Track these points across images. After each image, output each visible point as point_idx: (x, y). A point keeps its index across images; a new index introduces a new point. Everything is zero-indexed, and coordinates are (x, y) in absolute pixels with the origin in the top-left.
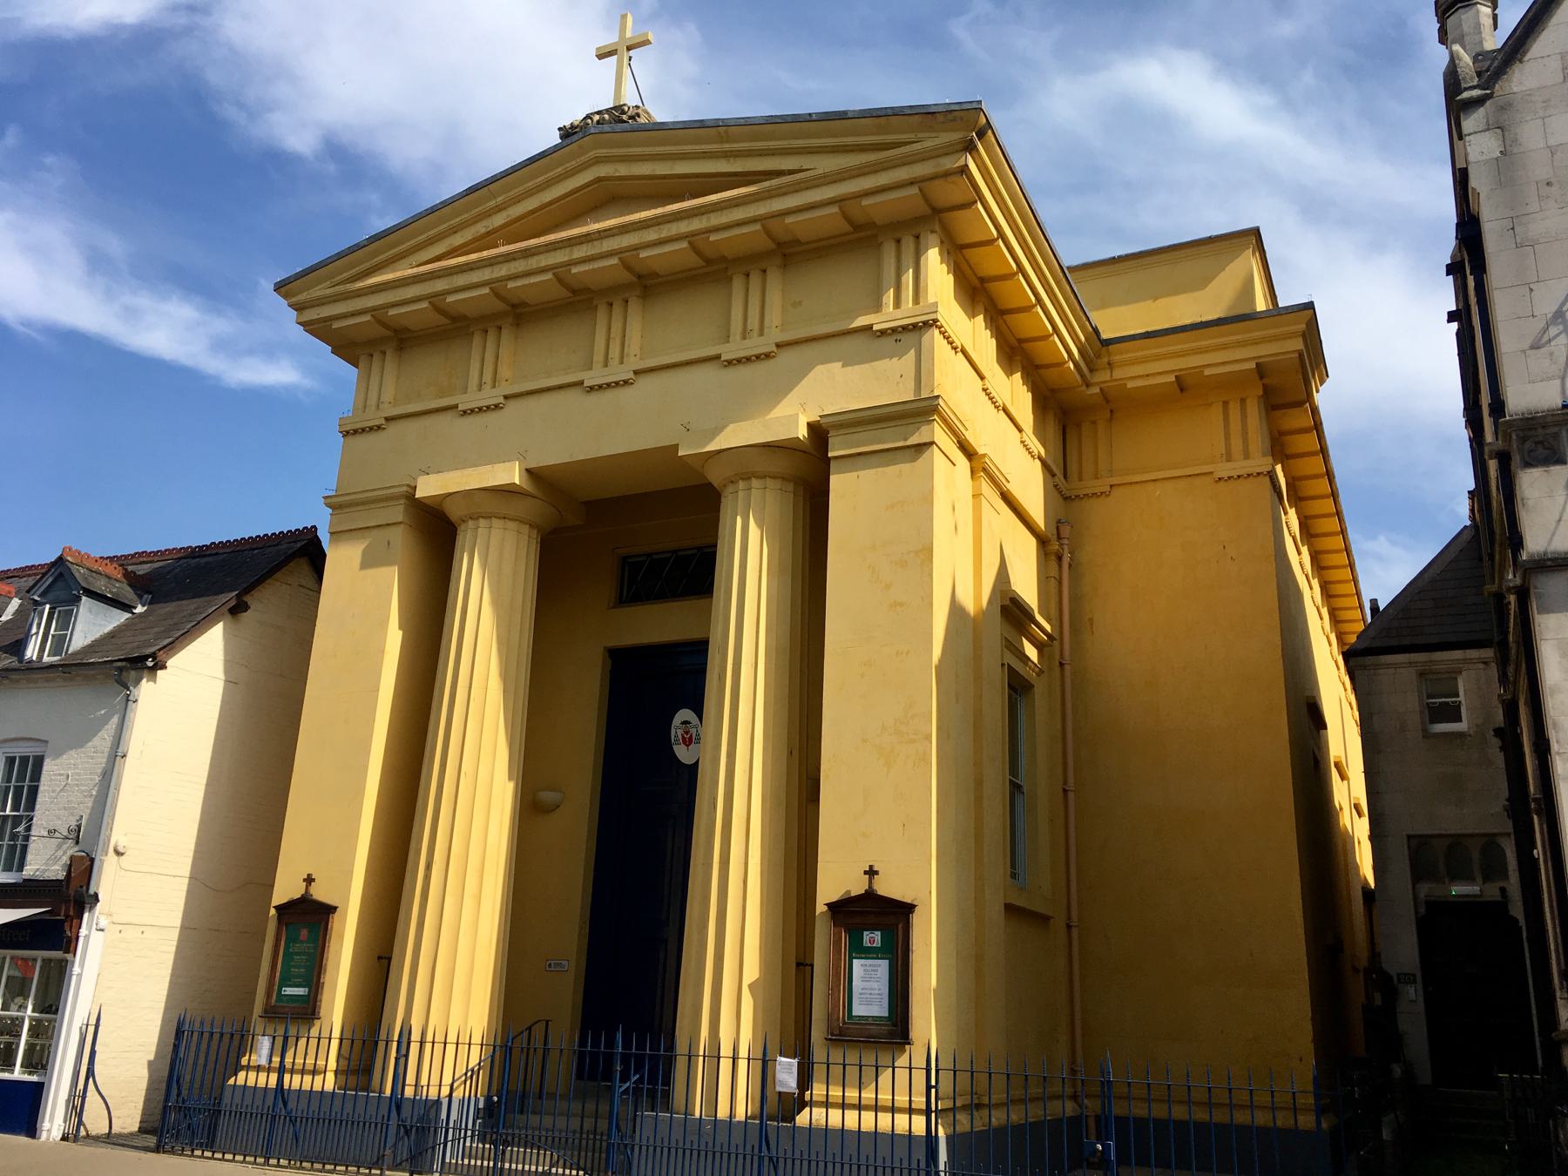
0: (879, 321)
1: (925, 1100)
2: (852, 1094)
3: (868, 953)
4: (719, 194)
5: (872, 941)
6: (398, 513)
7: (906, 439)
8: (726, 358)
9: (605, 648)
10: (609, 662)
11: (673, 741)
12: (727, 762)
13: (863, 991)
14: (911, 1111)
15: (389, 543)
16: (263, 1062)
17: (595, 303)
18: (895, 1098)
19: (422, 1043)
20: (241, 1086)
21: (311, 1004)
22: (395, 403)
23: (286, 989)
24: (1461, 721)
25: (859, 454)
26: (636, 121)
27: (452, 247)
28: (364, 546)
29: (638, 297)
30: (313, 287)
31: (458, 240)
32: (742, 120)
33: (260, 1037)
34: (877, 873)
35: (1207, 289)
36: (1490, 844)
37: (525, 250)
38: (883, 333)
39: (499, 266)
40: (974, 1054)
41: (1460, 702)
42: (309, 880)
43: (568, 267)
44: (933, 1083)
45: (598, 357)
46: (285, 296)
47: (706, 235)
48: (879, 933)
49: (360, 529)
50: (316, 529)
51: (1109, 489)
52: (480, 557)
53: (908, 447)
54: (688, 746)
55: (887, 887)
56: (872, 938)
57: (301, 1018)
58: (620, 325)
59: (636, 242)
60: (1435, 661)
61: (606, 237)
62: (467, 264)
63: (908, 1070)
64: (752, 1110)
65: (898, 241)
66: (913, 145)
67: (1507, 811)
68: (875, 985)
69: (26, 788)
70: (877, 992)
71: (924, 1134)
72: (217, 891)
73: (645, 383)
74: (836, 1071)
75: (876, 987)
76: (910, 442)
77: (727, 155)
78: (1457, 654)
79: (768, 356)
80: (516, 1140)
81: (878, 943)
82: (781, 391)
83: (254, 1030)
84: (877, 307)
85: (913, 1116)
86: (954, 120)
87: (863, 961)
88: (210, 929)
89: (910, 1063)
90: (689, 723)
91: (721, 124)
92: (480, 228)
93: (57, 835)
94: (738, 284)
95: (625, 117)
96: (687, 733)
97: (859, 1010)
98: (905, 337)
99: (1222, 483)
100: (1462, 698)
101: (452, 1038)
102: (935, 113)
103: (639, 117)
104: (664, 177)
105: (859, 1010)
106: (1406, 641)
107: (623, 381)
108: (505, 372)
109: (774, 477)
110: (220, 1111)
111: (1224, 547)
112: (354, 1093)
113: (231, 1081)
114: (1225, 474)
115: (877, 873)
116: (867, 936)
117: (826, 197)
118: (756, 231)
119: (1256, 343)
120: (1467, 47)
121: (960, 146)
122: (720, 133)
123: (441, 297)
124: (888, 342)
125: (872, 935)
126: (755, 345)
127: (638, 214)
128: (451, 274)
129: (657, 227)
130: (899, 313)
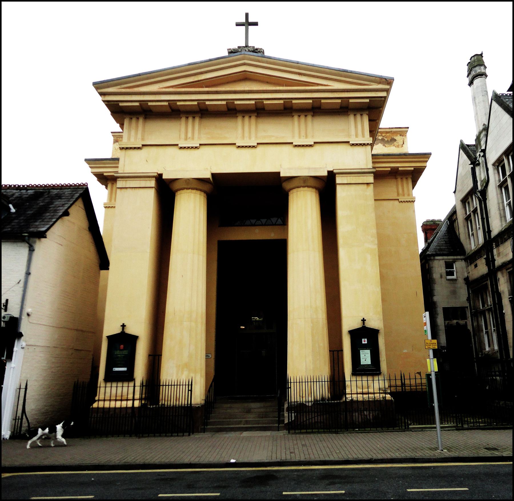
1: (346, 391)
6: (152, 183)
24: (454, 276)
29: (367, 114)
41: (454, 270)
46: (97, 89)
56: (365, 341)
66: (369, 86)
79: (311, 146)
88: (55, 347)
120: (244, 48)
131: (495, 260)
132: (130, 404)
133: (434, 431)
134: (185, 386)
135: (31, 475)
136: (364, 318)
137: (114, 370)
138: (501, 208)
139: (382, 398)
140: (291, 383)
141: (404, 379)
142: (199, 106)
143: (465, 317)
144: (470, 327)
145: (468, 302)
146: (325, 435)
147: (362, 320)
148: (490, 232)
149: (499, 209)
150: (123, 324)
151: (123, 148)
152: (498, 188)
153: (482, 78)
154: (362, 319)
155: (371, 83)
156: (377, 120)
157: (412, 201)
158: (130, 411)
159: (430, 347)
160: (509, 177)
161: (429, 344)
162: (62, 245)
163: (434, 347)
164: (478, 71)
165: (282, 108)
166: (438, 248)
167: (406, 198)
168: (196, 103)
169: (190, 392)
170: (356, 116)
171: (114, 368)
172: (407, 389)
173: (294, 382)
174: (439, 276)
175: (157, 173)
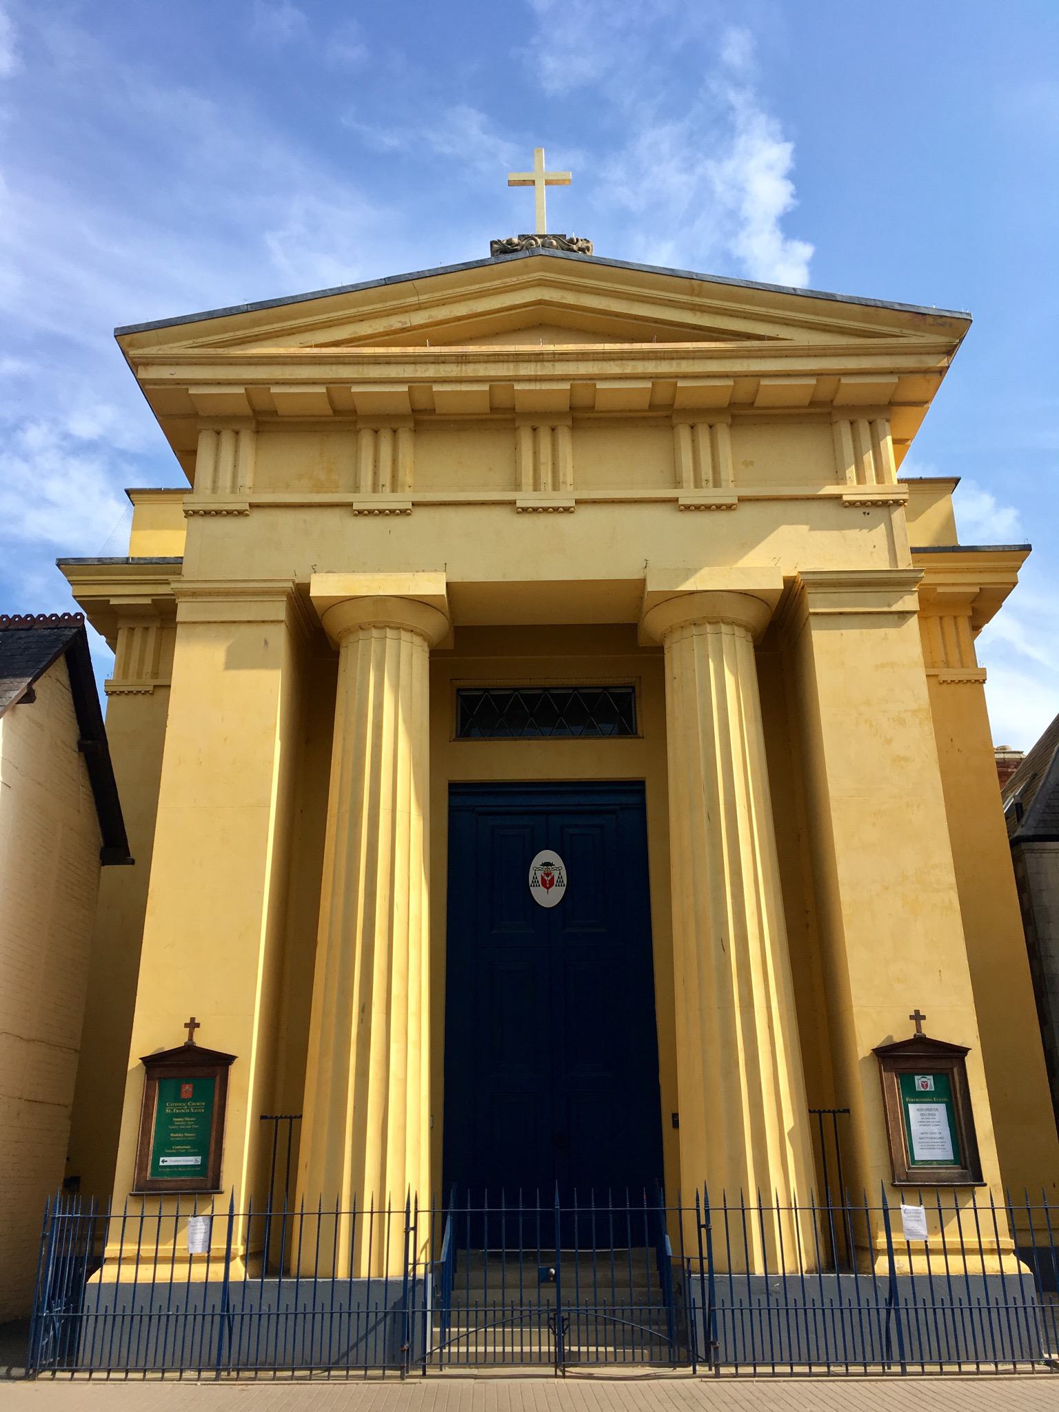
0: (850, 490)
2: (148, 1249)
3: (922, 1097)
4: (694, 343)
5: (925, 1085)
6: (279, 610)
7: (890, 606)
8: (683, 503)
11: (530, 883)
12: (732, 903)
13: (924, 1136)
14: (999, 1251)
15: (266, 643)
16: (198, 1249)
17: (675, 421)
18: (964, 1240)
19: (356, 1214)
20: (109, 1284)
21: (210, 1174)
22: (254, 489)
23: (166, 1159)
25: (841, 613)
26: (585, 253)
27: (357, 335)
28: (229, 644)
30: (165, 343)
31: (365, 329)
32: (718, 278)
33: (190, 1219)
34: (198, 1025)
35: (917, 521)
37: (462, 356)
38: (852, 504)
39: (424, 366)
40: (305, 1198)
42: (193, 1025)
43: (268, 386)
44: (703, 1230)
45: (527, 477)
47: (675, 380)
48: (931, 1077)
49: (222, 622)
51: (152, 689)
52: (731, 671)
53: (891, 613)
54: (548, 888)
55: (206, 1040)
56: (925, 1082)
57: (199, 1194)
58: (549, 451)
59: (597, 372)
61: (559, 361)
62: (631, 352)
63: (973, 1210)
64: (807, 1263)
65: (237, 433)
68: (935, 1129)
70: (938, 1136)
71: (222, 1280)
72: (29, 1041)
73: (585, 513)
74: (133, 1224)
75: (936, 1131)
76: (895, 608)
77: (694, 308)
80: (582, 1316)
81: (931, 1087)
82: (748, 543)
83: (390, 1207)
84: (840, 479)
85: (930, 1257)
86: (943, 325)
87: (918, 1106)
89: (992, 1203)
91: (695, 277)
92: (395, 322)
94: (366, 440)
95: (575, 247)
96: (548, 875)
97: (920, 1154)
98: (874, 511)
99: (945, 685)
101: (716, 1202)
102: (925, 314)
103: (588, 250)
104: (617, 315)
105: (920, 1154)
107: (389, 510)
108: (406, 477)
109: (739, 625)
110: (82, 1317)
111: (952, 740)
112: (296, 1280)
113: (94, 1278)
114: (949, 679)
115: (198, 1025)
116: (918, 1080)
117: (734, 370)
118: (727, 386)
119: (980, 572)
121: (944, 349)
122: (692, 285)
123: (346, 385)
124: (857, 514)
125: (923, 1080)
126: (387, 500)
127: (602, 345)
128: (363, 364)
129: (619, 362)
130: (862, 488)
132: (217, 1272)
134: (778, 1206)
137: (161, 1164)
139: (806, 1272)
141: (707, 1211)
142: (331, 402)
151: (195, 513)
154: (196, 1022)
156: (908, 440)
157: (944, 681)
158: (161, 1300)
162: (10, 787)
165: (485, 407)
167: (963, 674)
168: (240, 390)
170: (713, 428)
171: (161, 1159)
172: (952, 1243)
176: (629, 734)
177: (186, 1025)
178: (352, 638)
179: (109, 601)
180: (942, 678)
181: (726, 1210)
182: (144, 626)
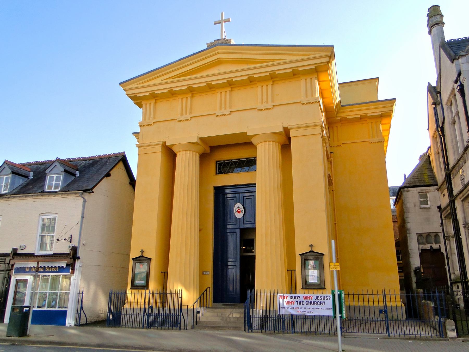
6: (160, 148)
9: (214, 187)
10: (214, 190)
36: (436, 235)
50: (125, 152)
60: (410, 190)
67: (441, 227)
69: (46, 227)
78: (428, 188)
89: (395, 296)
90: (240, 207)
93: (66, 240)
96: (239, 210)
97: (144, 282)
100: (428, 199)
101: (113, 292)
105: (144, 282)
106: (418, 184)
115: (313, 246)
131: (453, 190)
133: (348, 337)
135: (71, 348)
136: (311, 244)
137: (136, 282)
138: (454, 143)
140: (175, 294)
143: (437, 242)
144: (443, 251)
145: (441, 228)
146: (427, 342)
147: (310, 246)
148: (448, 165)
149: (452, 144)
150: (142, 250)
152: (451, 125)
153: (438, 26)
155: (315, 53)
159: (334, 269)
160: (456, 115)
161: (333, 266)
163: (337, 269)
164: (434, 21)
166: (412, 180)
167: (376, 139)
169: (180, 299)
173: (174, 294)
174: (413, 205)
175: (163, 141)
176: (253, 171)
177: (310, 246)
178: (172, 148)
179: (347, 117)
180: (370, 142)
181: (353, 295)
182: (371, 122)
